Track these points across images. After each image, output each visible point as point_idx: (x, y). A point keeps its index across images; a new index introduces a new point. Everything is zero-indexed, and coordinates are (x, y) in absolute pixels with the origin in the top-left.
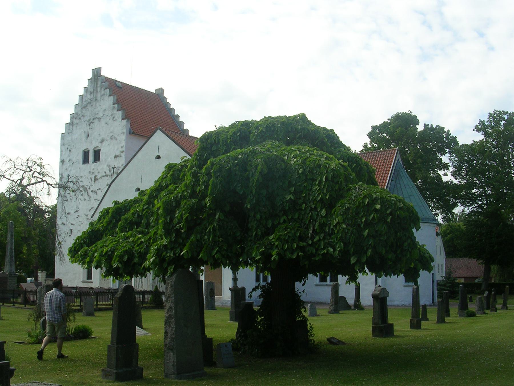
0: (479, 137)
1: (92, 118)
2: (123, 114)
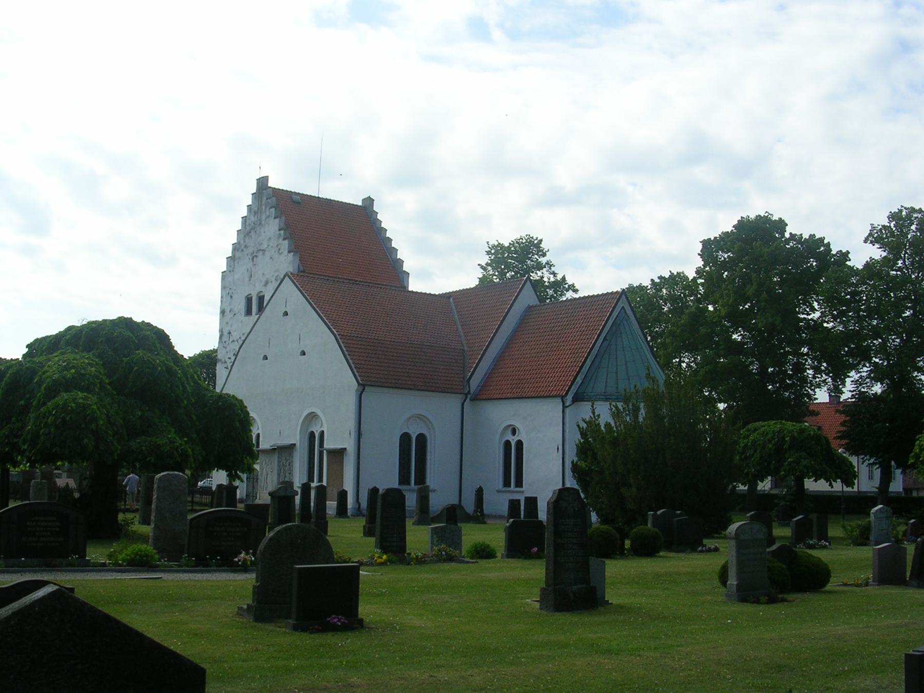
0: (877, 253)
2: (290, 245)
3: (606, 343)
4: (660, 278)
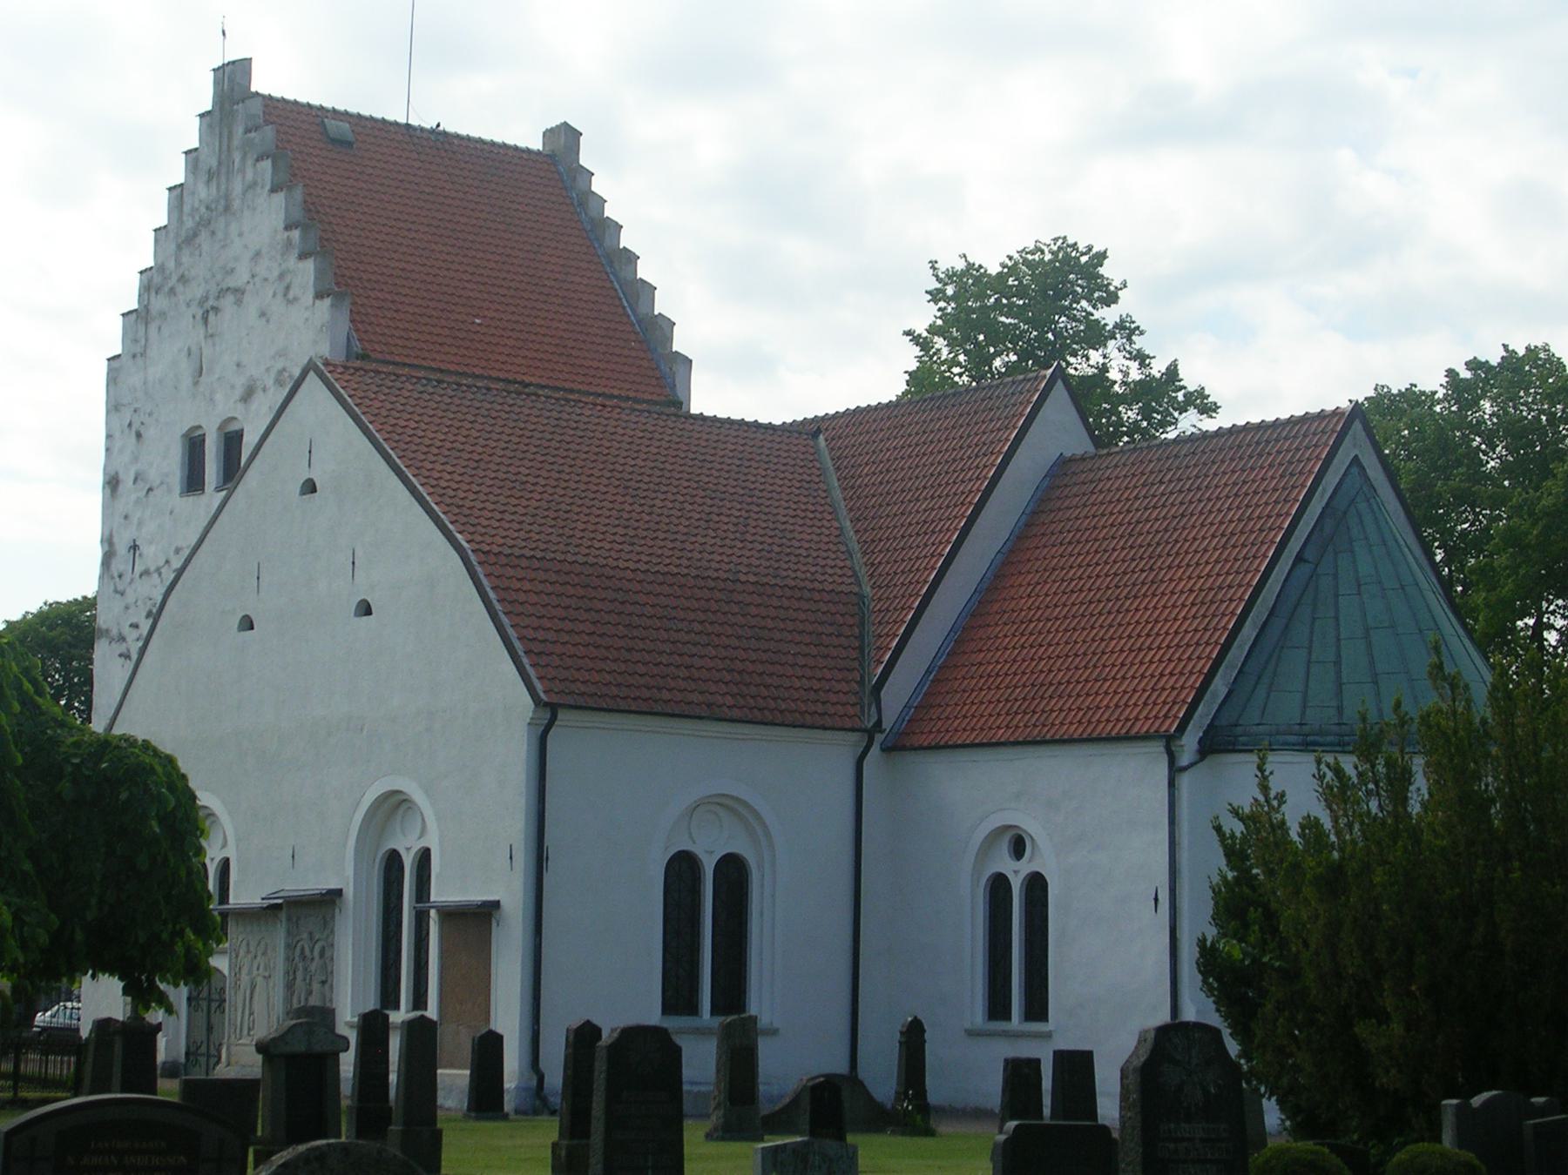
1: (214, 290)
3: (1305, 569)
4: (1473, 365)
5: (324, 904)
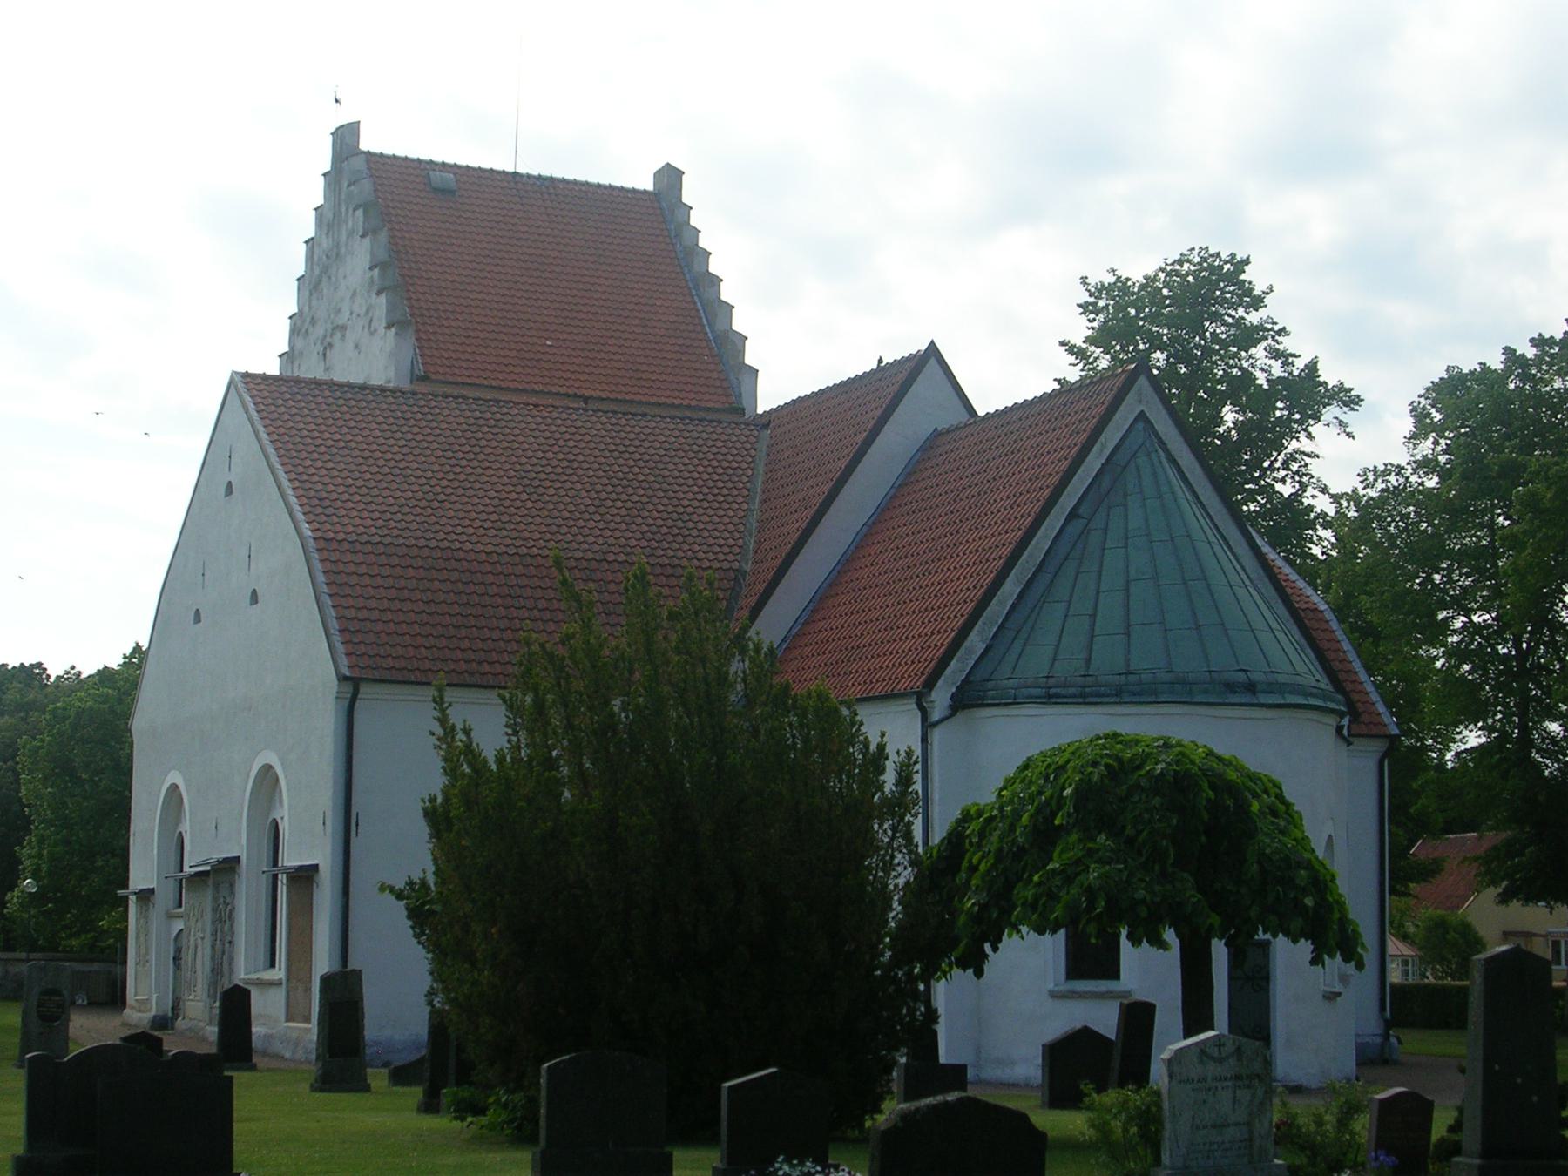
2: (391, 308)
3: (1078, 525)
4: (1539, 342)
5: (229, 866)
